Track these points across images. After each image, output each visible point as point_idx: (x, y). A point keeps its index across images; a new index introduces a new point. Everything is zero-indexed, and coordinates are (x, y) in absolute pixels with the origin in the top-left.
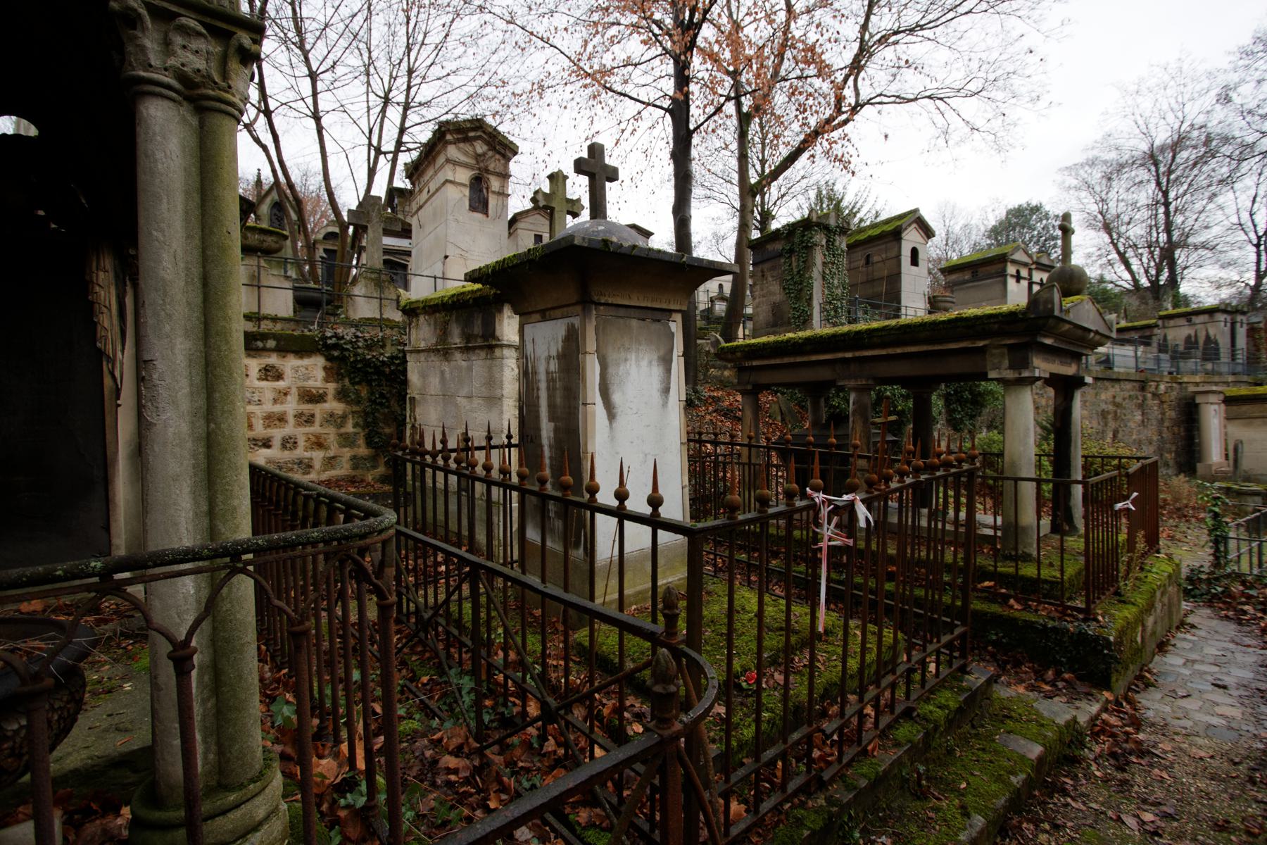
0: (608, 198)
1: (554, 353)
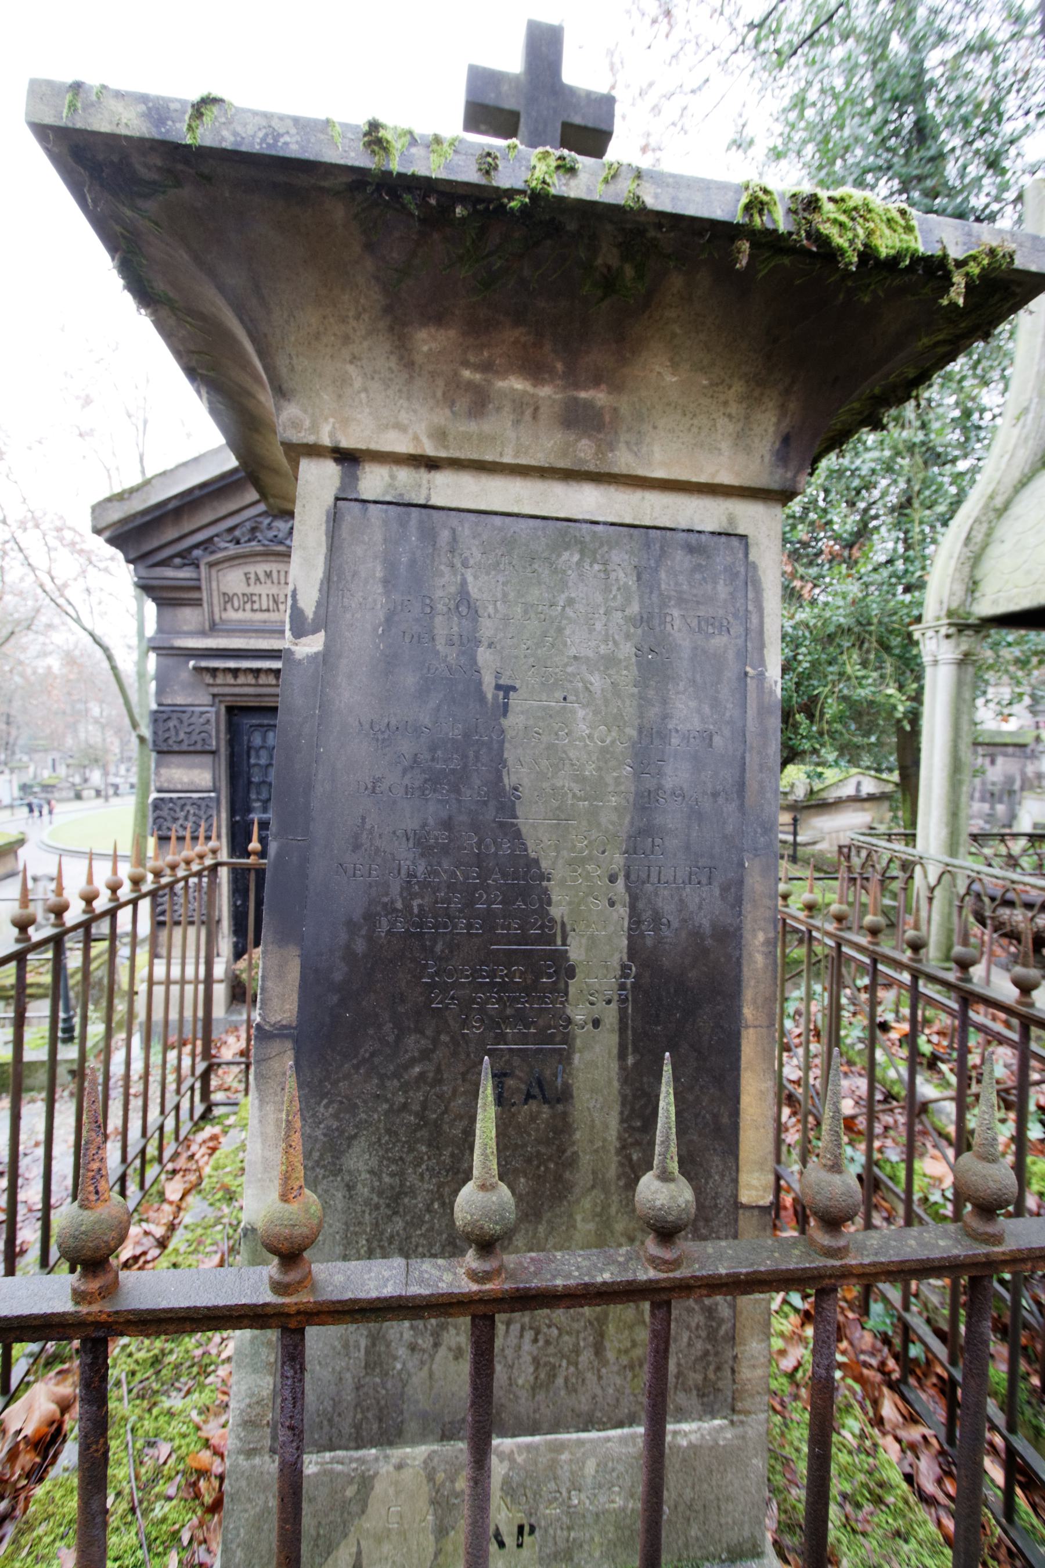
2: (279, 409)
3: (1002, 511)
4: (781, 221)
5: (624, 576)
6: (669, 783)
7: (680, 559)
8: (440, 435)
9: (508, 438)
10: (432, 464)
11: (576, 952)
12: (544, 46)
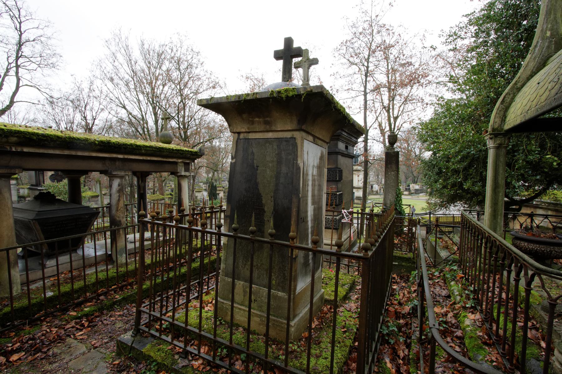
0: (341, 103)
1: (316, 165)
2: (303, 94)
3: (519, 90)
4: (275, 95)
5: (275, 147)
6: (281, 182)
7: (284, 143)
8: (248, 128)
9: (257, 127)
10: (249, 132)
11: (266, 209)
12: (289, 42)
